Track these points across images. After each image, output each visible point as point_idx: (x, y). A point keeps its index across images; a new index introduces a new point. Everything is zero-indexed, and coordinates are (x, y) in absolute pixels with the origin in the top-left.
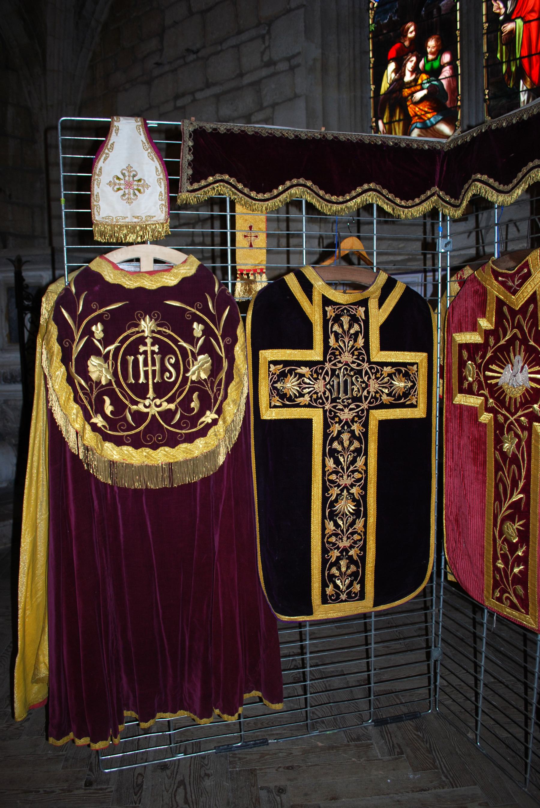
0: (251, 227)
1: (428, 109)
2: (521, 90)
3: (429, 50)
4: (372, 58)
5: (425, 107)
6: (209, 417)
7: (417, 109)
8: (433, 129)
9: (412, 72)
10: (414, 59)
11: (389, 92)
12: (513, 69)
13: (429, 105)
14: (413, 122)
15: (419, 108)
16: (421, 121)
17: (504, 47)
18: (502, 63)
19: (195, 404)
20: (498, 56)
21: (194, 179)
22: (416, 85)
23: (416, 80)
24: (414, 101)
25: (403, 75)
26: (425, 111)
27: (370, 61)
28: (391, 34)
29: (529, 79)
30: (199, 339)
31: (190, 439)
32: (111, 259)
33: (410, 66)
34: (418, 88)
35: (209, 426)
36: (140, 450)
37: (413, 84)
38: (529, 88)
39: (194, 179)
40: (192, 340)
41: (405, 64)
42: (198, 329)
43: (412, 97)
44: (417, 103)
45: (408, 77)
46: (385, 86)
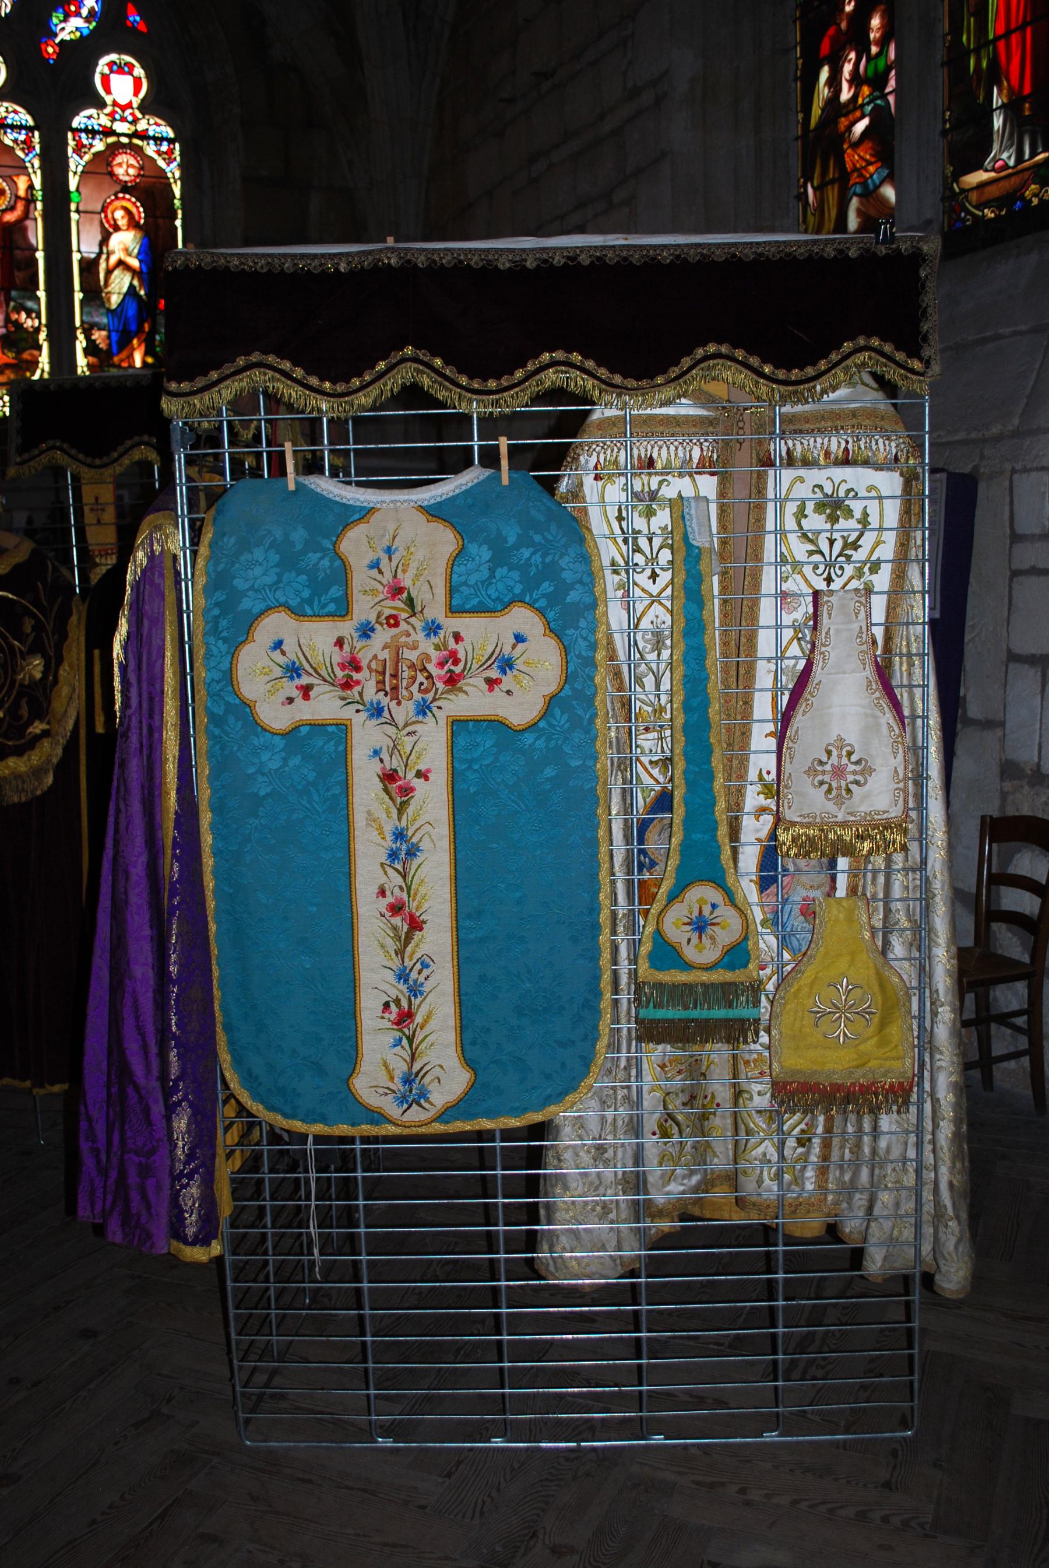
0: (97, 499)
1: (871, 155)
2: (994, 106)
3: (872, 36)
4: (801, 57)
5: (866, 152)
6: (38, 727)
7: (856, 157)
8: (877, 197)
9: (850, 82)
10: (852, 55)
11: (823, 122)
12: (984, 64)
13: (872, 148)
14: (851, 182)
15: (859, 156)
16: (862, 180)
17: (972, 20)
18: (967, 53)
19: (24, 711)
20: (964, 38)
21: (22, 450)
22: (855, 109)
23: (854, 98)
24: (853, 140)
25: (838, 91)
26: (866, 161)
27: (797, 65)
28: (824, 7)
29: (1005, 83)
30: (28, 635)
31: (19, 752)
32: (726, 392)
33: (848, 68)
34: (858, 114)
35: (37, 738)
36: (26, 757)
37: (851, 107)
38: (1005, 101)
39: (22, 450)
40: (20, 637)
41: (842, 67)
42: (28, 625)
43: (851, 131)
44: (856, 145)
45: (845, 95)
46: (816, 112)
